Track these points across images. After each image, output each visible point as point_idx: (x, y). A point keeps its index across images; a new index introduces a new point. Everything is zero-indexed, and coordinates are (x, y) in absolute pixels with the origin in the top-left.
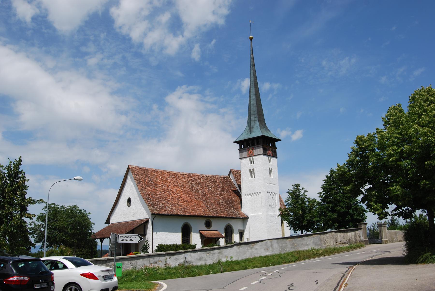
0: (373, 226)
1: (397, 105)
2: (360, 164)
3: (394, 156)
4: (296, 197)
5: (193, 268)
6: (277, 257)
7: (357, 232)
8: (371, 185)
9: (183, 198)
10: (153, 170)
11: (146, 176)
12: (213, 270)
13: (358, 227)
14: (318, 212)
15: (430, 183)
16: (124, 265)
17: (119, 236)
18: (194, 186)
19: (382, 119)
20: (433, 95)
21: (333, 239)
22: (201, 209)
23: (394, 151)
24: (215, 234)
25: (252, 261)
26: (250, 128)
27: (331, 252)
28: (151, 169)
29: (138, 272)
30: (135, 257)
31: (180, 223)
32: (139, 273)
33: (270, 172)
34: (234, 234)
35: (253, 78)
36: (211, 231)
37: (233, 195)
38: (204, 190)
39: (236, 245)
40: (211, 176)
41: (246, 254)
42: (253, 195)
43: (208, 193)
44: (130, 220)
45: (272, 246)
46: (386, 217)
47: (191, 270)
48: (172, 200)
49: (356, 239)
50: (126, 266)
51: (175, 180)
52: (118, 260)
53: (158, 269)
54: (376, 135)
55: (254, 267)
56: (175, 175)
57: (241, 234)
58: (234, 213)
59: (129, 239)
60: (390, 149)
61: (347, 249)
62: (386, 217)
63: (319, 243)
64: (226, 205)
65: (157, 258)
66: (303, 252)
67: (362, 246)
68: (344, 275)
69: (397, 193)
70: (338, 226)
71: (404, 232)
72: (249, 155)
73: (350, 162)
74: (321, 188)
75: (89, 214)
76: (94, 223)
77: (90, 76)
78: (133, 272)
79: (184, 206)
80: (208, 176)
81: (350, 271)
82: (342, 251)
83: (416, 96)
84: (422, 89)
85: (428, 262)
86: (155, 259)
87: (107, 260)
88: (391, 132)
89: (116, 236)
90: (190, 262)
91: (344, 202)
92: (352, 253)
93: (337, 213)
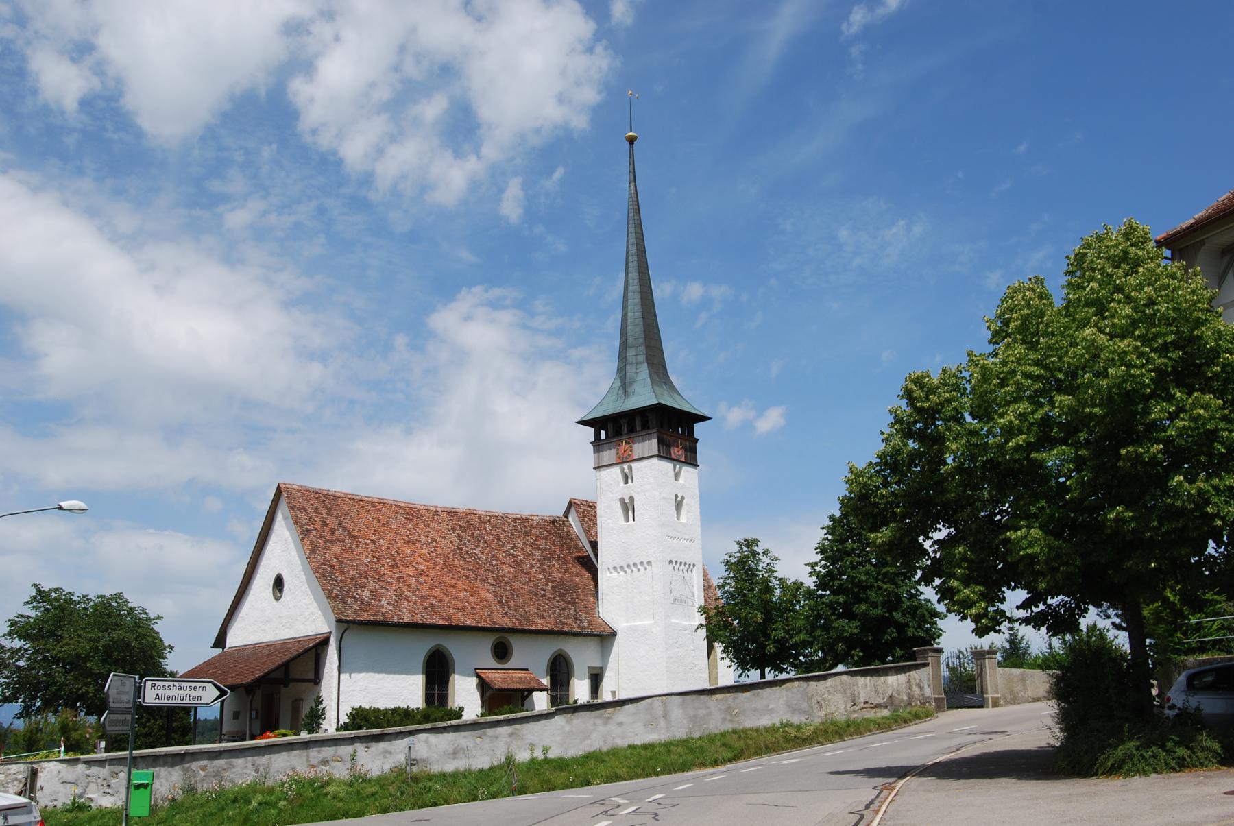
0: (959, 659)
1: (1030, 279)
2: (917, 462)
3: (1021, 433)
4: (748, 575)
5: (430, 780)
6: (680, 749)
7: (915, 674)
8: (952, 529)
9: (431, 576)
10: (349, 496)
11: (328, 515)
12: (488, 788)
13: (918, 659)
14: (807, 618)
15: (1138, 515)
16: (234, 770)
17: (149, 684)
18: (465, 544)
19: (987, 324)
20: (1143, 243)
21: (845, 693)
22: (482, 609)
23: (1022, 417)
24: (520, 678)
25: (607, 759)
26: (625, 384)
27: (836, 732)
28: (344, 494)
29: (271, 791)
30: (265, 746)
31: (422, 647)
32: (272, 795)
33: (679, 505)
34: (576, 680)
35: (634, 247)
36: (510, 671)
37: (574, 570)
38: (494, 555)
39: (561, 712)
40: (514, 517)
41: (590, 739)
42: (628, 571)
43: (504, 563)
44: (278, 638)
45: (665, 716)
46: (997, 628)
47: (425, 786)
48: (400, 582)
49: (912, 693)
50: (241, 772)
51: (410, 526)
52: (218, 754)
53: (328, 783)
54: (966, 374)
55: (609, 779)
56: (411, 513)
57: (596, 679)
58: (576, 619)
59: (182, 693)
60: (1011, 412)
61: (884, 723)
62: (997, 628)
63: (805, 706)
64: (554, 598)
65: (328, 750)
66: (755, 734)
67: (928, 715)
68: (862, 817)
69: (1032, 550)
70: (860, 658)
71: (1054, 675)
72: (619, 457)
73: (888, 458)
74: (816, 550)
75: (157, 621)
76: (172, 645)
77: (231, 257)
78: (255, 792)
79: (433, 601)
80: (507, 517)
81: (882, 803)
82: (870, 731)
83: (1090, 253)
84: (1106, 231)
85: (1130, 770)
86: (324, 753)
87: (185, 753)
88: (1014, 359)
89: (136, 682)
90: (425, 761)
91: (880, 588)
92: (899, 735)
93: (859, 620)
